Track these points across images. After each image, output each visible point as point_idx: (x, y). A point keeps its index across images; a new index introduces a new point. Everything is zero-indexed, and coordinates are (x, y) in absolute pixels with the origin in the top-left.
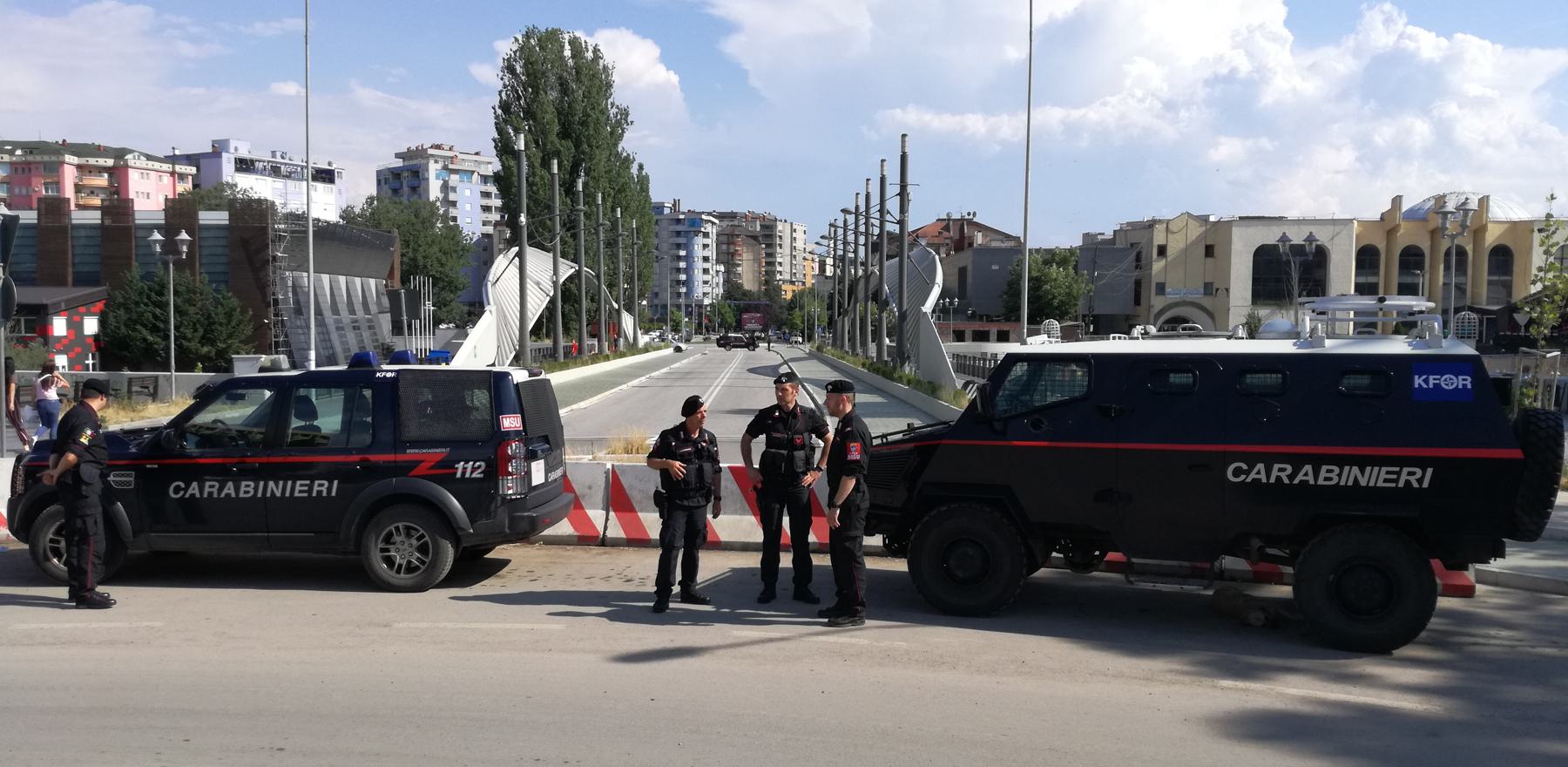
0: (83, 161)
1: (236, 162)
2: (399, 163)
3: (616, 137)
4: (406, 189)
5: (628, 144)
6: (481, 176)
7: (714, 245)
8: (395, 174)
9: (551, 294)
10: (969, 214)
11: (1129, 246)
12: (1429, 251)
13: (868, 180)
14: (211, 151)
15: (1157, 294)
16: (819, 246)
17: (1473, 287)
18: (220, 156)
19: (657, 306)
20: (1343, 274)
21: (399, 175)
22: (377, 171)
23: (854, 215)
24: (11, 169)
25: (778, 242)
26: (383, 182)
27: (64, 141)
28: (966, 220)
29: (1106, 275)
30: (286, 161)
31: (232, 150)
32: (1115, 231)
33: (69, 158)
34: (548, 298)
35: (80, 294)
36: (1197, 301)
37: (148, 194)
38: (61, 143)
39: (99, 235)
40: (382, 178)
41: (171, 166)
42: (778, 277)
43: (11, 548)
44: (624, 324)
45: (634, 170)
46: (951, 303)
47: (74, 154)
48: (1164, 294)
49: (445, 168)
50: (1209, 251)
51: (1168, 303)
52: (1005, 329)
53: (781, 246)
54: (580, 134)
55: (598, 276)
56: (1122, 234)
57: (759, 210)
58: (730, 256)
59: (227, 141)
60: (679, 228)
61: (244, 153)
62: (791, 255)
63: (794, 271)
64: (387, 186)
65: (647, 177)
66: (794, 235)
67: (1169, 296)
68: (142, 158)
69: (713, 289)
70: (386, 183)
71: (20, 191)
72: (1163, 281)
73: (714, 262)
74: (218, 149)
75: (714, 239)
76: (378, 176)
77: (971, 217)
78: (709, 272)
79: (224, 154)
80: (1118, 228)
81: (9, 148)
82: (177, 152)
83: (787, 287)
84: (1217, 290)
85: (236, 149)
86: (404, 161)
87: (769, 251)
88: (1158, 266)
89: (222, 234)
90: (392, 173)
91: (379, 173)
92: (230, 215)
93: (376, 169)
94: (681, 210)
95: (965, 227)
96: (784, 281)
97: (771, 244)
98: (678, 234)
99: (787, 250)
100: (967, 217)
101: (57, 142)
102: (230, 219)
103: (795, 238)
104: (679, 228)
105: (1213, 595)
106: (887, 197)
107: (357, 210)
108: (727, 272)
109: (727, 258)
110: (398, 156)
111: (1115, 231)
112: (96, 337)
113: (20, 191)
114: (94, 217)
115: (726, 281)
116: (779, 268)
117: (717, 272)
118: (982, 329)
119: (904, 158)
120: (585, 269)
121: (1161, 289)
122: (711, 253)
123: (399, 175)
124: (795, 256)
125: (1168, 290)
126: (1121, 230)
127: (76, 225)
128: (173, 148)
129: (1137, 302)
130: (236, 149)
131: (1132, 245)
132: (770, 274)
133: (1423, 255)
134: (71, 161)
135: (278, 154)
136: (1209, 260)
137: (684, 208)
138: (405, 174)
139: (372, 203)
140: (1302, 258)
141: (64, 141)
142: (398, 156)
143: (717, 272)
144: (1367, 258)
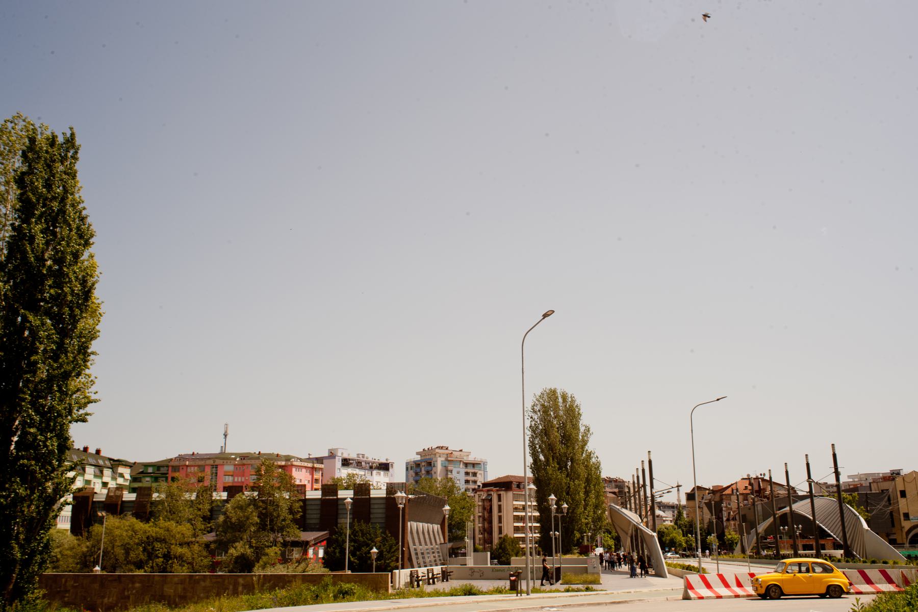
1: (342, 461)
2: (418, 458)
3: (585, 443)
4: (423, 472)
5: (590, 447)
6: (464, 463)
8: (417, 464)
10: (761, 475)
11: (881, 492)
13: (649, 452)
15: (904, 520)
21: (419, 464)
22: (406, 463)
24: (234, 468)
26: (409, 468)
27: (260, 452)
28: (760, 478)
29: (874, 509)
30: (365, 459)
35: (318, 535)
37: (301, 480)
40: (409, 466)
46: (784, 529)
48: (909, 520)
49: (447, 460)
51: (912, 525)
57: (283, 452)
61: (346, 456)
64: (412, 471)
67: (912, 521)
68: (299, 460)
70: (411, 469)
71: (238, 479)
72: (907, 512)
74: (332, 455)
76: (406, 465)
77: (762, 476)
81: (233, 457)
82: (311, 457)
85: (342, 454)
86: (421, 456)
88: (902, 502)
89: (319, 502)
91: (407, 464)
95: (761, 483)
100: (760, 476)
110: (418, 453)
112: (323, 558)
113: (238, 479)
114: (318, 495)
118: (808, 543)
121: (907, 516)
123: (419, 464)
125: (911, 517)
127: (124, 501)
129: (893, 526)
130: (342, 454)
131: (882, 491)
140: (562, 514)
141: (260, 452)
142: (418, 453)
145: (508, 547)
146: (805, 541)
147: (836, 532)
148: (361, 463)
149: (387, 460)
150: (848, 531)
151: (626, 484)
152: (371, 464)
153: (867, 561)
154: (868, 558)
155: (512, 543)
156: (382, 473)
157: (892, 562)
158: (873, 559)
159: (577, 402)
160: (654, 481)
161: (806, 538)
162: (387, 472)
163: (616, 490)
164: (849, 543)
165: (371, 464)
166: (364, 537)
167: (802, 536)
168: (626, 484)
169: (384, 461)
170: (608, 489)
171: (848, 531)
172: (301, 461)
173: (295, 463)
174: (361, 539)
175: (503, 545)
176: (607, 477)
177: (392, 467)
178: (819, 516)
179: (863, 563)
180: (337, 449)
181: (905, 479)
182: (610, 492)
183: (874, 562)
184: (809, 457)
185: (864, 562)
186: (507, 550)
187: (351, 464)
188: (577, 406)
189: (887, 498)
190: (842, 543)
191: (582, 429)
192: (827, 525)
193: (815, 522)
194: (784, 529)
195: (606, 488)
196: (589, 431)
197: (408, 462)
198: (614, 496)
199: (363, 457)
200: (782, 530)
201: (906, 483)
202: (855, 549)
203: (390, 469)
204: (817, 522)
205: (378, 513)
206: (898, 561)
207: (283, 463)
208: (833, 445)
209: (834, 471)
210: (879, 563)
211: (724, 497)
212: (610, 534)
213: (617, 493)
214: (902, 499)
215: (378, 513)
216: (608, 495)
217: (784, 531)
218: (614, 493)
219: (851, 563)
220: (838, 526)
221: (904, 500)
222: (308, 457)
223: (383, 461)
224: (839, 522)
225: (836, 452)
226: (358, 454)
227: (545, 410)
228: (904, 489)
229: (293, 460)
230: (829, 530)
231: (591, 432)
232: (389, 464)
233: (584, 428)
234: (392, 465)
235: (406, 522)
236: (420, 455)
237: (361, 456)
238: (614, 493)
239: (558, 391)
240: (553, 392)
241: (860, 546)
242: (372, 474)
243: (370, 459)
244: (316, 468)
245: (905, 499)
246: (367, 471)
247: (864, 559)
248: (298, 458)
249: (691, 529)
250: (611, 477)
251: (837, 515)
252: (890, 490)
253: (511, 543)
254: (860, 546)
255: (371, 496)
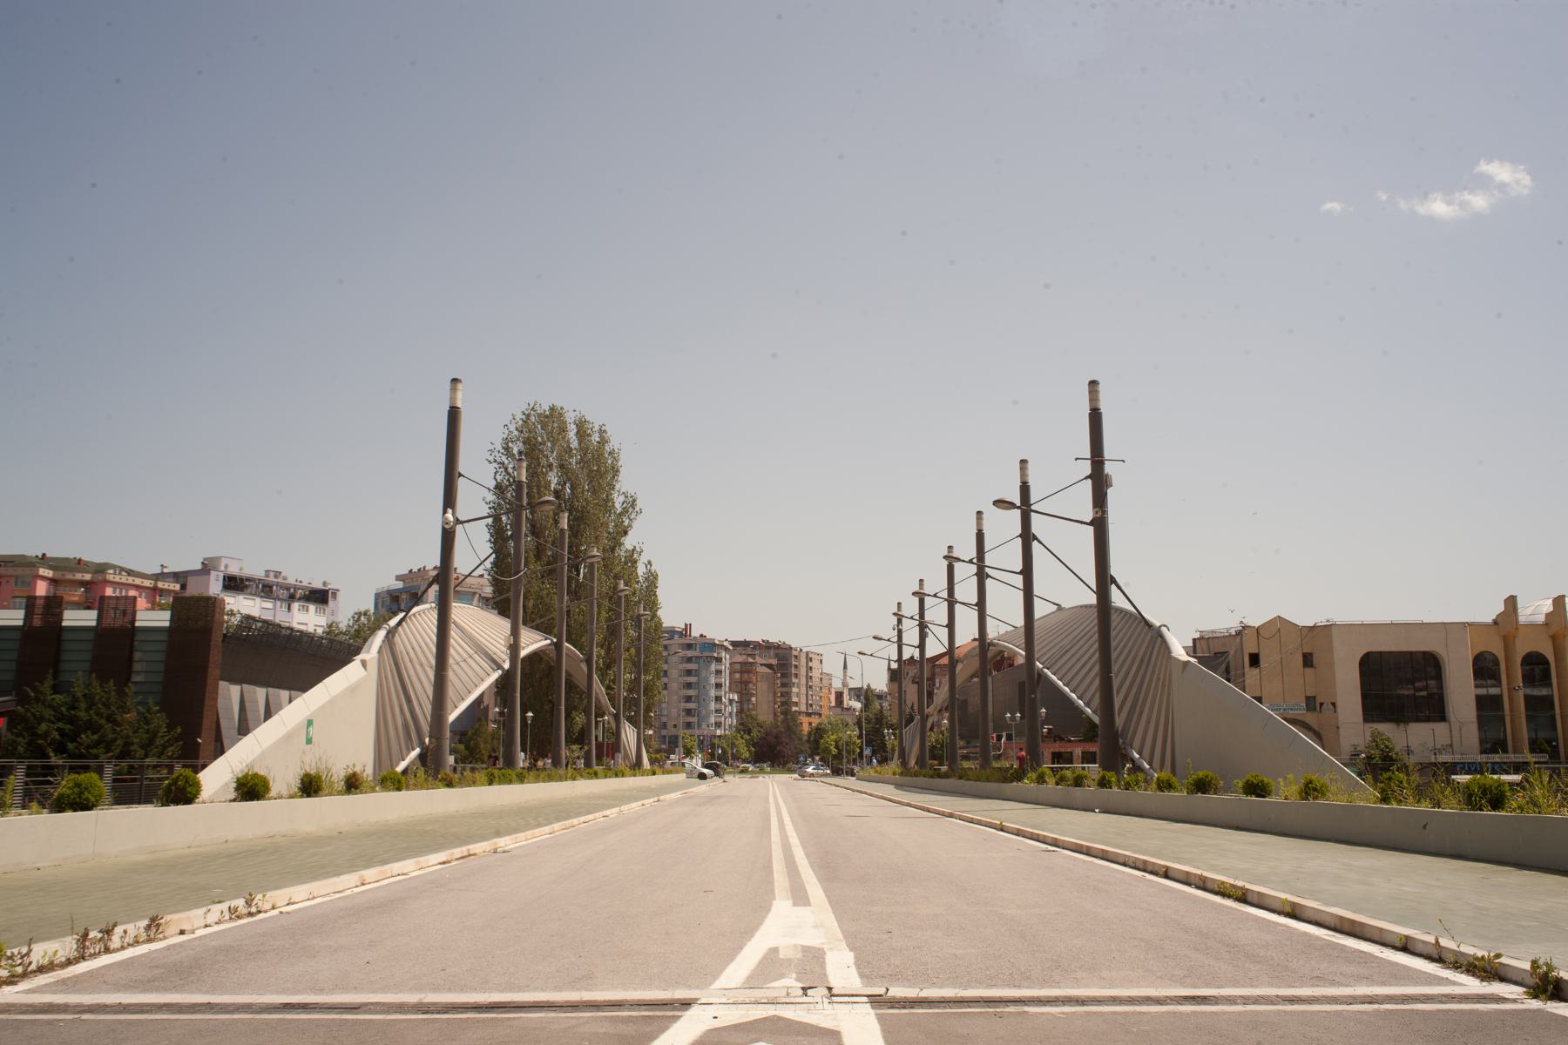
0: (58, 575)
2: (400, 585)
6: (483, 598)
7: (728, 672)
9: (507, 666)
12: (1503, 654)
13: (455, 381)
14: (200, 568)
16: (879, 642)
17: (1561, 709)
18: (209, 574)
19: (665, 737)
20: (1461, 691)
21: (398, 597)
22: (376, 594)
23: (1017, 513)
25: (794, 663)
27: (44, 555)
30: (280, 580)
31: (222, 568)
32: (1194, 640)
33: (43, 572)
34: (496, 675)
36: (1300, 718)
38: (40, 556)
39: (161, 680)
41: (153, 582)
42: (794, 709)
43: (1098, 701)
44: (623, 736)
45: (641, 570)
46: (1013, 718)
47: (50, 568)
50: (1308, 660)
52: (1091, 750)
53: (796, 676)
54: (578, 532)
55: (589, 662)
56: (1204, 643)
58: (743, 685)
59: (218, 559)
60: (690, 653)
61: (234, 570)
62: (807, 685)
63: (810, 702)
65: (655, 577)
66: (810, 664)
69: (725, 719)
73: (727, 690)
74: (207, 568)
75: (728, 666)
78: (721, 699)
79: (212, 572)
80: (1197, 635)
82: (165, 570)
83: (805, 720)
84: (1322, 704)
85: (226, 566)
86: (404, 583)
87: (785, 680)
90: (391, 595)
91: (377, 596)
92: (172, 616)
93: (375, 592)
94: (693, 634)
96: (800, 713)
97: (787, 674)
98: (689, 660)
99: (803, 671)
101: (37, 556)
102: (171, 620)
103: (811, 668)
104: (690, 653)
105: (169, 631)
106: (987, 547)
107: (343, 627)
108: (740, 702)
109: (743, 686)
111: (1194, 640)
115: (740, 712)
116: (795, 699)
117: (731, 701)
119: (1095, 418)
120: (566, 644)
122: (725, 680)
123: (398, 597)
124: (811, 687)
126: (1201, 638)
128: (162, 566)
130: (226, 566)
131: (1215, 654)
132: (787, 703)
133: (1547, 663)
134: (46, 574)
135: (272, 574)
136: (1309, 671)
137: (695, 633)
138: (404, 596)
139: (359, 619)
141: (44, 555)
142: (398, 578)
143: (731, 701)
144: (1485, 668)
145: (482, 746)
146: (1058, 747)
147: (1085, 692)
148: (271, 587)
149: (324, 584)
150: (1118, 658)
151: (794, 653)
152: (292, 590)
153: (1174, 780)
154: (1178, 770)
155: (493, 739)
156: (312, 607)
157: (1294, 789)
158: (1201, 774)
159: (614, 443)
160: (461, 482)
161: (1062, 739)
162: (322, 606)
163: (774, 662)
164: (1119, 722)
165: (292, 590)
166: (91, 712)
167: (1054, 736)
168: (794, 653)
169: (320, 586)
170: (759, 660)
171: (1118, 658)
172: (129, 575)
173: (110, 578)
174: (82, 715)
175: (472, 743)
176: (763, 641)
177: (335, 598)
178: (1041, 653)
179: (1160, 788)
180: (220, 557)
181: (1260, 632)
182: (762, 665)
183: (1202, 786)
184: (1030, 466)
185: (1165, 786)
186: (480, 751)
187: (247, 587)
188: (610, 453)
189: (1224, 666)
190: (1096, 719)
191: (618, 501)
192: (1061, 674)
193: (1034, 664)
194: (1013, 718)
195: (757, 657)
196: (633, 504)
197: (379, 593)
198: (769, 671)
199: (276, 577)
200: (1008, 719)
201: (1260, 638)
202: (1137, 743)
203: (331, 602)
204: (1038, 663)
205: (146, 667)
206: (1326, 779)
207: (88, 577)
208: (1093, 384)
209: (1088, 471)
210: (1226, 790)
211: (937, 670)
212: (749, 734)
213: (775, 667)
214: (1253, 669)
215: (146, 667)
216: (758, 670)
217: (1013, 723)
218: (770, 666)
219: (1115, 789)
220: (1092, 661)
221: (1255, 671)
222: (159, 571)
223: (318, 585)
224: (1095, 652)
225: (1104, 407)
226: (267, 572)
227: (531, 451)
228: (1256, 652)
229: (111, 571)
230: (1060, 679)
231: (637, 509)
232: (328, 591)
233: (622, 498)
234: (334, 595)
235: (210, 681)
236: (403, 581)
237: (272, 574)
238: (770, 666)
239: (570, 417)
240: (555, 415)
241: (1156, 730)
242: (289, 609)
243: (291, 581)
244: (162, 590)
245: (1258, 670)
246: (278, 603)
247: (1165, 775)
248: (122, 569)
249: (878, 726)
250: (771, 641)
251: (1091, 622)
252: (1232, 652)
253: (489, 738)
254: (1156, 730)
255: (137, 624)
